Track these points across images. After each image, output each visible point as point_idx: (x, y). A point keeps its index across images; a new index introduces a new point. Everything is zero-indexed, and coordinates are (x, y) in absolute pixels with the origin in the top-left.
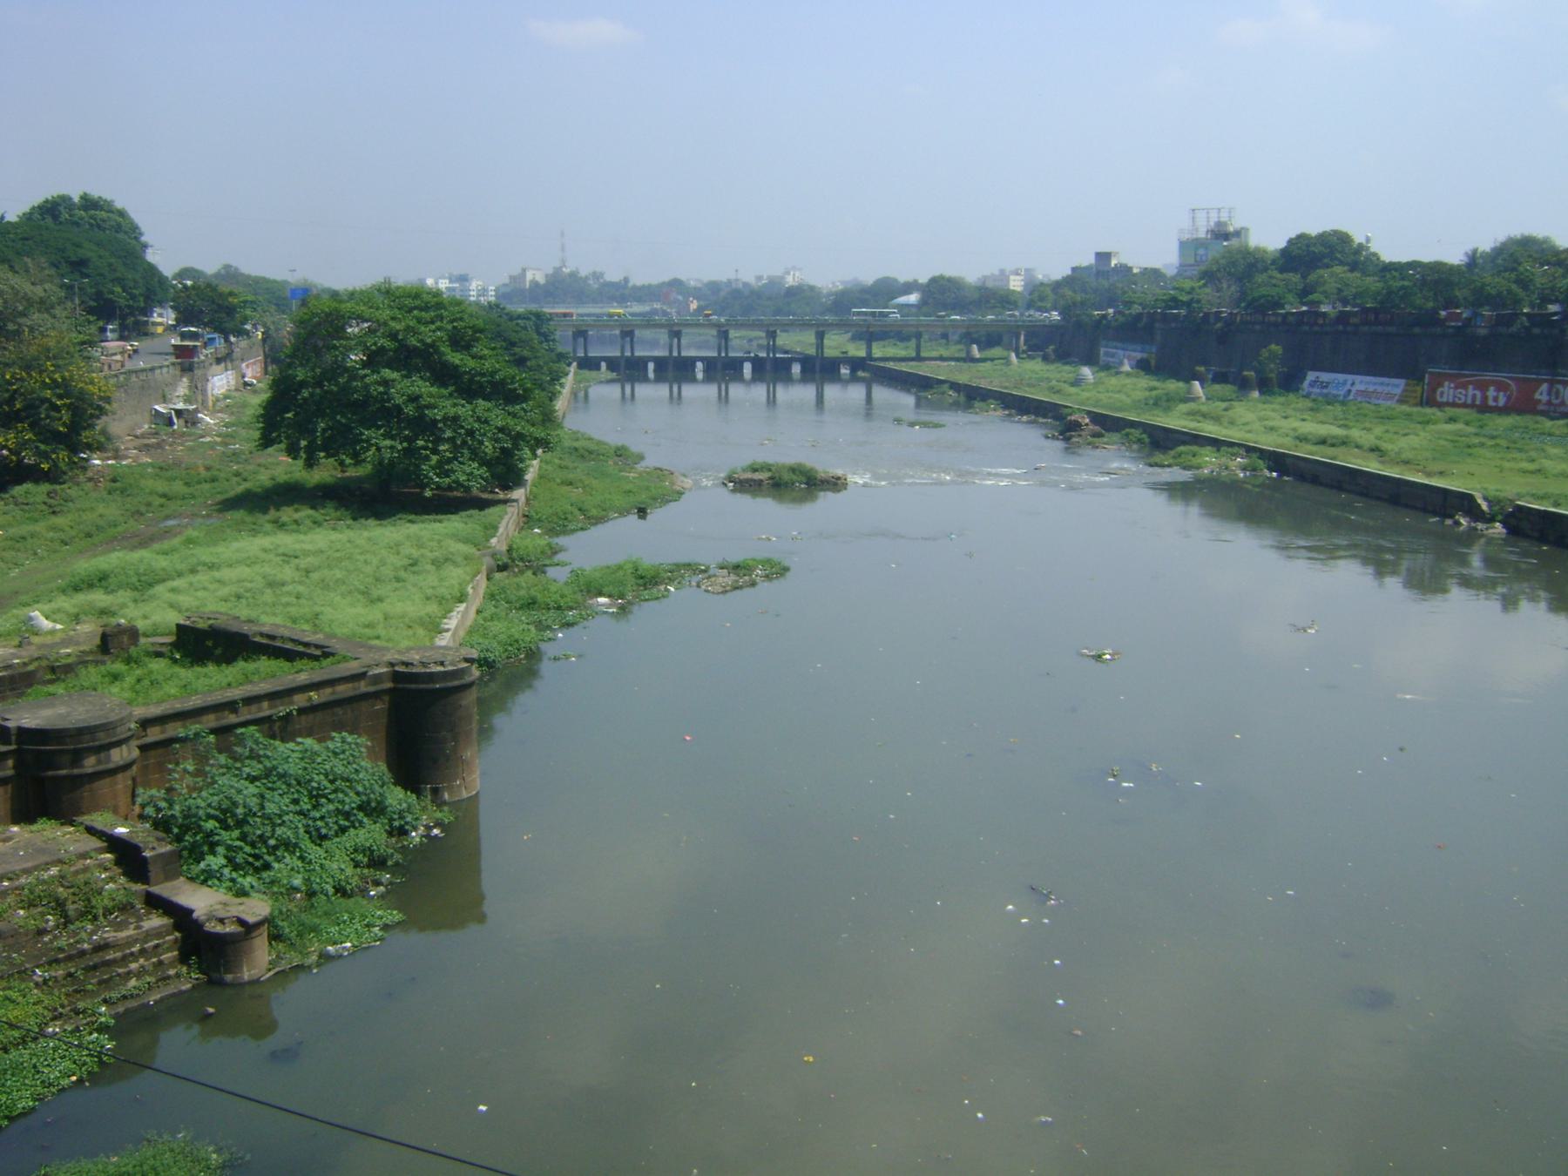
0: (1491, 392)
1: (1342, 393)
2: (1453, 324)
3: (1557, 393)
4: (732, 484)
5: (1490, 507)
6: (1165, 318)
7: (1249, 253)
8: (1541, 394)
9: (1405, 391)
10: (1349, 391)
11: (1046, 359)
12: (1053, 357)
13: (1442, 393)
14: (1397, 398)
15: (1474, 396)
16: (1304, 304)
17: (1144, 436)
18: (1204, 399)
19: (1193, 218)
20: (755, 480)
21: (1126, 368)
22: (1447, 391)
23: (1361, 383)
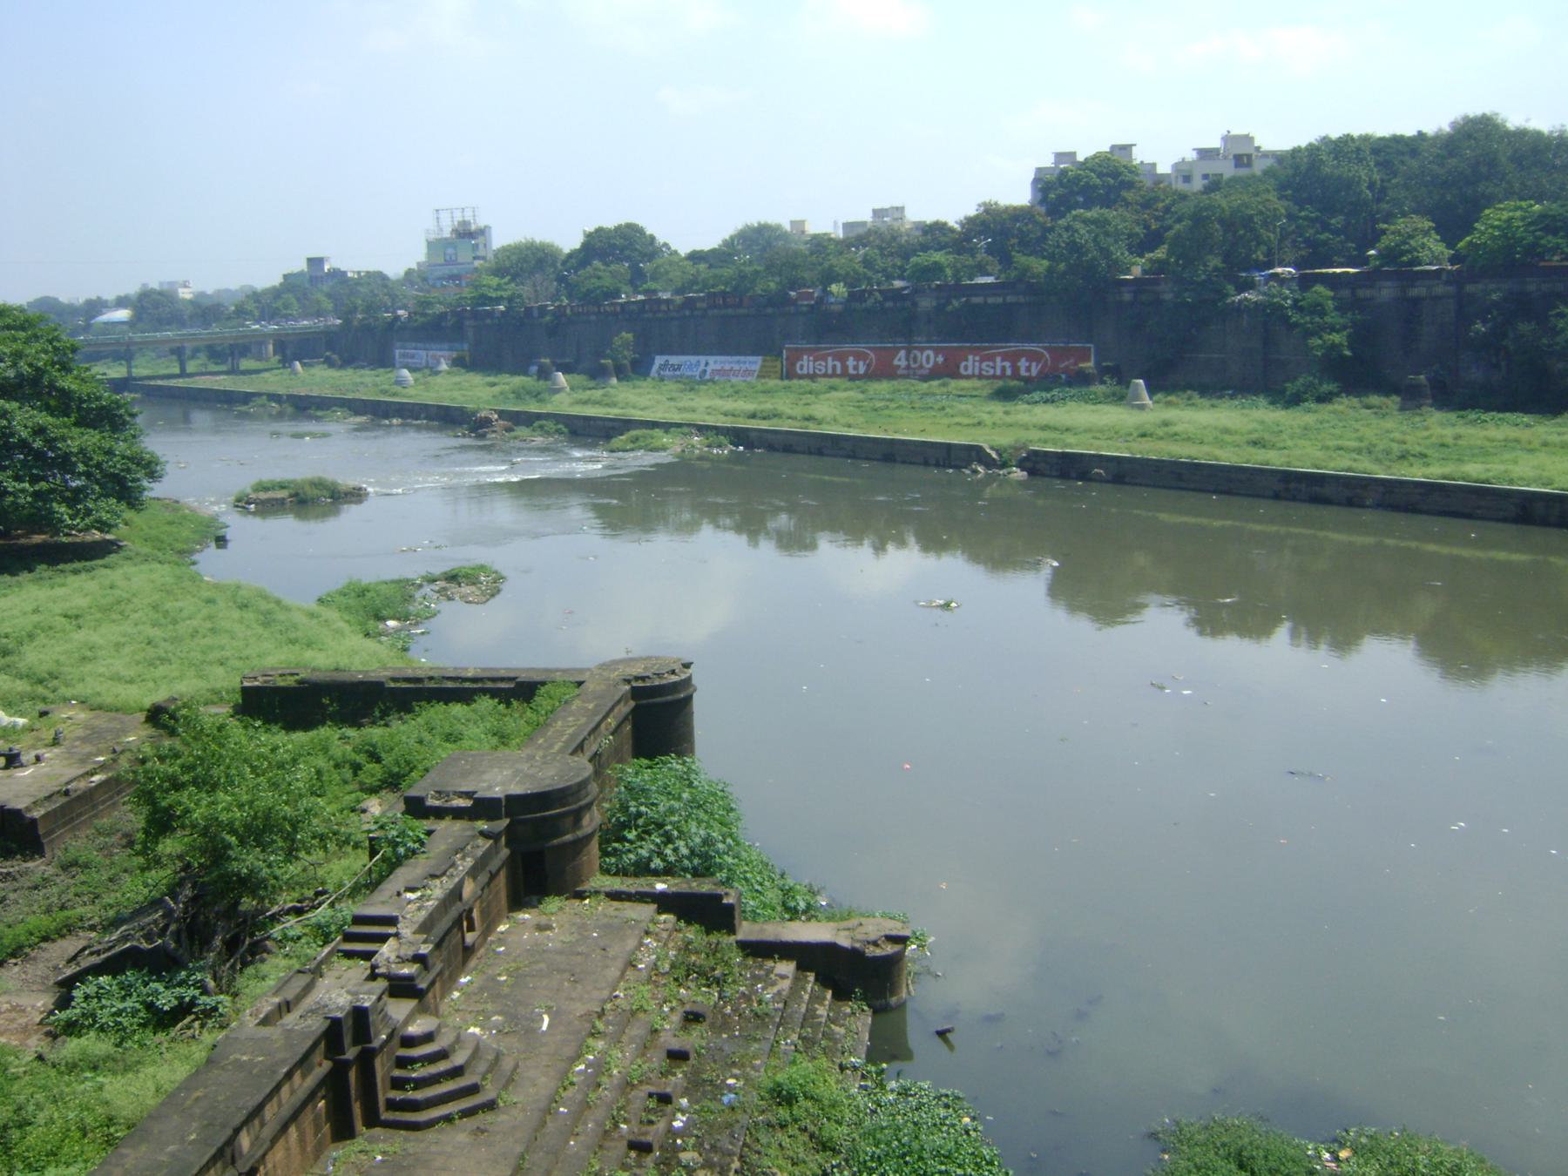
0: (851, 362)
1: (698, 373)
2: (806, 303)
3: (915, 360)
4: (252, 506)
5: (1000, 455)
6: (475, 315)
7: (537, 248)
8: (900, 360)
9: (762, 366)
10: (705, 371)
11: (330, 363)
12: (339, 363)
13: (802, 367)
14: (756, 374)
15: (834, 367)
16: (640, 293)
17: (560, 426)
18: (568, 389)
19: (438, 218)
20: (277, 499)
21: (444, 367)
22: (806, 364)
23: (715, 362)
